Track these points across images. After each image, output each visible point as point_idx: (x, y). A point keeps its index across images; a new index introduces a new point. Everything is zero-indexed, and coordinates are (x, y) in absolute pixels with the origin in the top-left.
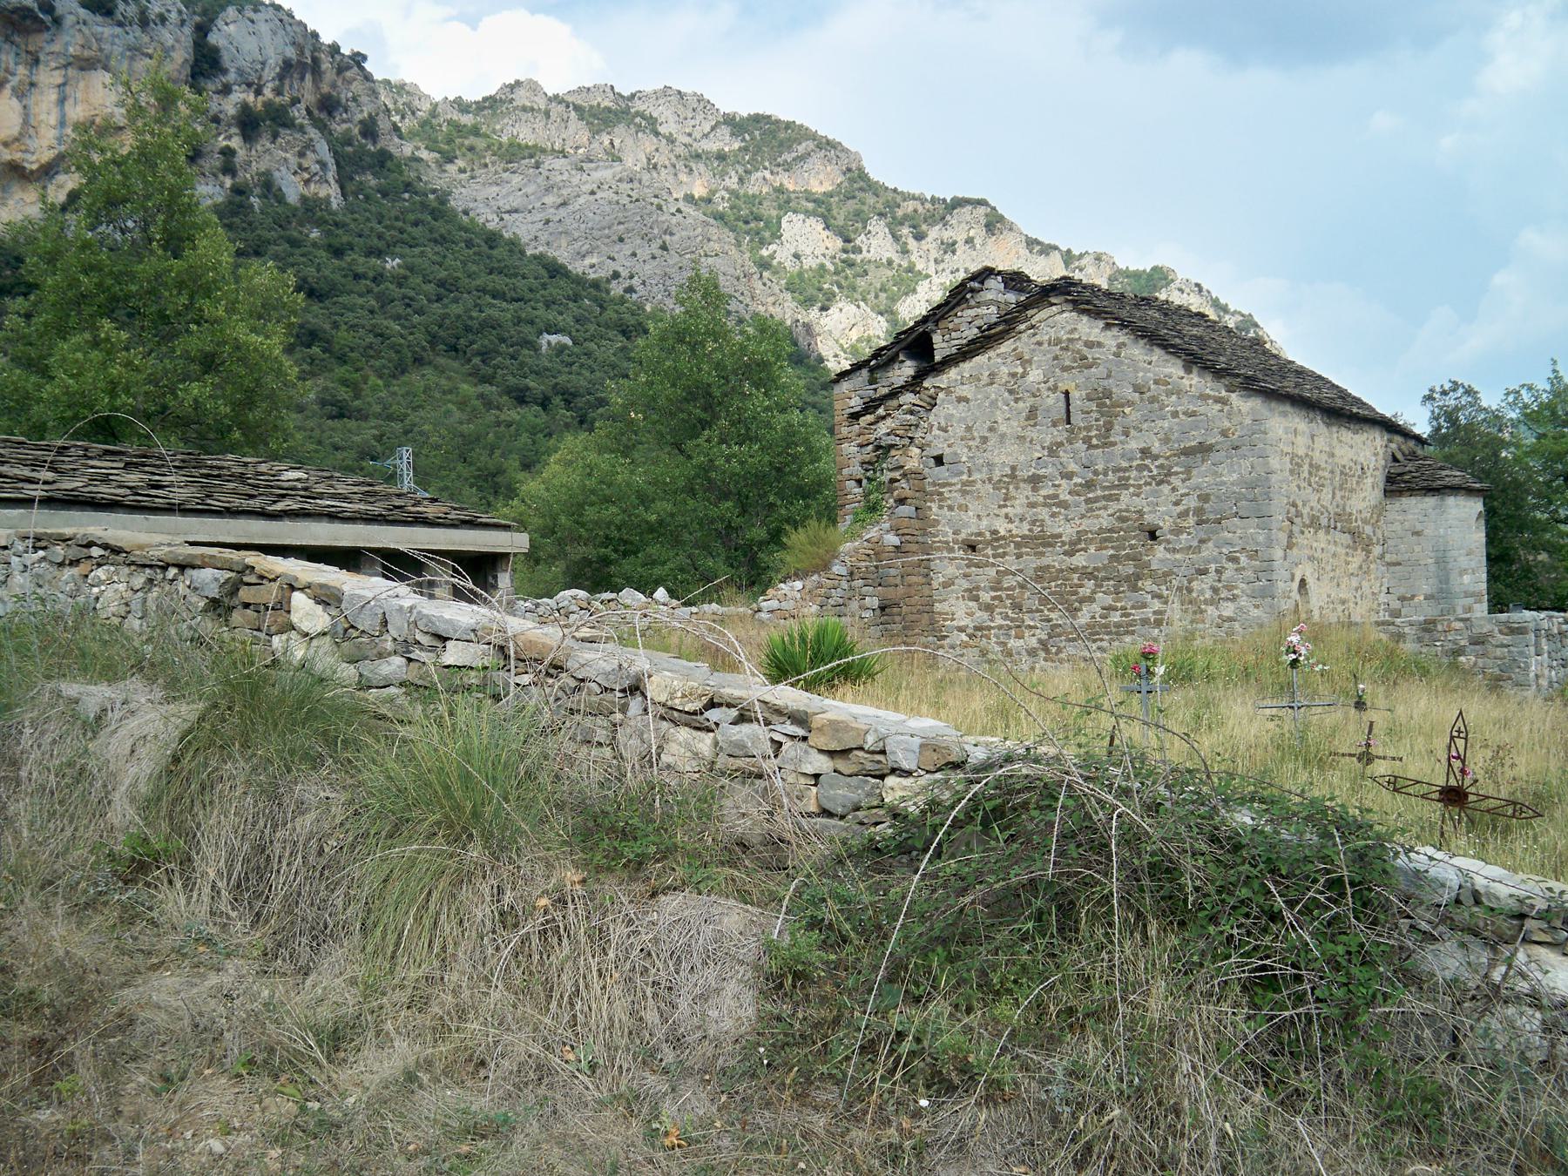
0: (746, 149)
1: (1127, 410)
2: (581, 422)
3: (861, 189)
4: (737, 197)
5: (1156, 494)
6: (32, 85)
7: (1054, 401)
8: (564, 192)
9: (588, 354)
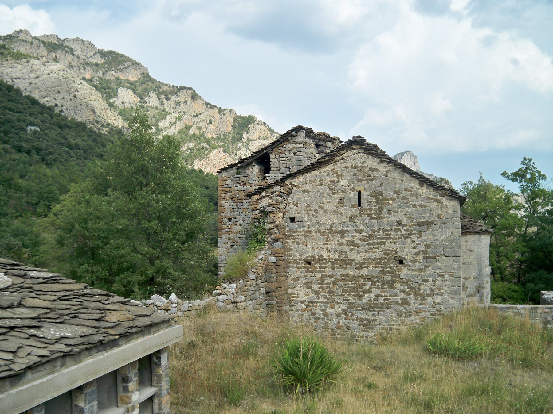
0: (106, 63)
1: (390, 202)
2: (43, 160)
3: (147, 81)
4: (102, 80)
5: (404, 243)
7: (353, 196)
8: (38, 73)
9: (46, 135)
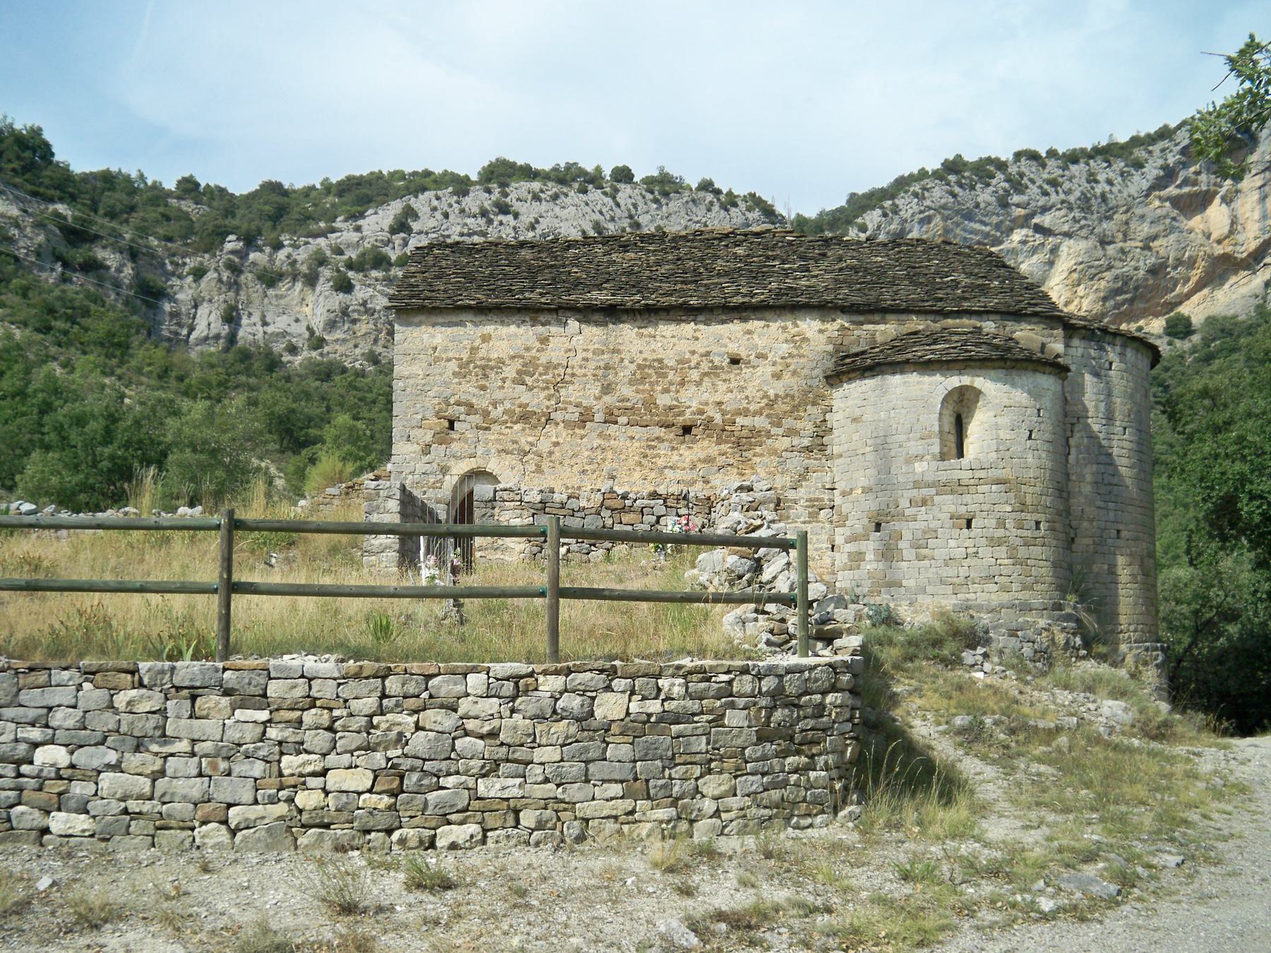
6: (1237, 191)
